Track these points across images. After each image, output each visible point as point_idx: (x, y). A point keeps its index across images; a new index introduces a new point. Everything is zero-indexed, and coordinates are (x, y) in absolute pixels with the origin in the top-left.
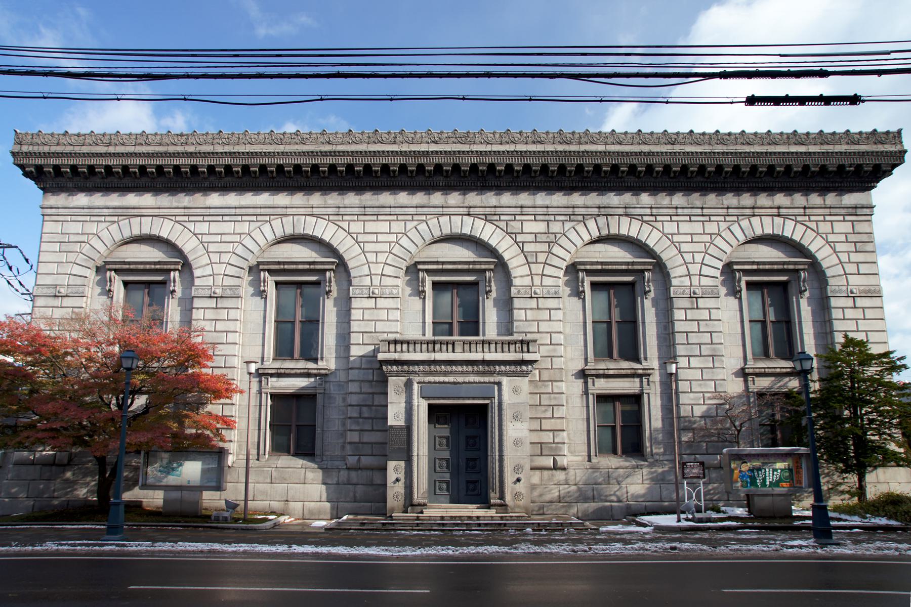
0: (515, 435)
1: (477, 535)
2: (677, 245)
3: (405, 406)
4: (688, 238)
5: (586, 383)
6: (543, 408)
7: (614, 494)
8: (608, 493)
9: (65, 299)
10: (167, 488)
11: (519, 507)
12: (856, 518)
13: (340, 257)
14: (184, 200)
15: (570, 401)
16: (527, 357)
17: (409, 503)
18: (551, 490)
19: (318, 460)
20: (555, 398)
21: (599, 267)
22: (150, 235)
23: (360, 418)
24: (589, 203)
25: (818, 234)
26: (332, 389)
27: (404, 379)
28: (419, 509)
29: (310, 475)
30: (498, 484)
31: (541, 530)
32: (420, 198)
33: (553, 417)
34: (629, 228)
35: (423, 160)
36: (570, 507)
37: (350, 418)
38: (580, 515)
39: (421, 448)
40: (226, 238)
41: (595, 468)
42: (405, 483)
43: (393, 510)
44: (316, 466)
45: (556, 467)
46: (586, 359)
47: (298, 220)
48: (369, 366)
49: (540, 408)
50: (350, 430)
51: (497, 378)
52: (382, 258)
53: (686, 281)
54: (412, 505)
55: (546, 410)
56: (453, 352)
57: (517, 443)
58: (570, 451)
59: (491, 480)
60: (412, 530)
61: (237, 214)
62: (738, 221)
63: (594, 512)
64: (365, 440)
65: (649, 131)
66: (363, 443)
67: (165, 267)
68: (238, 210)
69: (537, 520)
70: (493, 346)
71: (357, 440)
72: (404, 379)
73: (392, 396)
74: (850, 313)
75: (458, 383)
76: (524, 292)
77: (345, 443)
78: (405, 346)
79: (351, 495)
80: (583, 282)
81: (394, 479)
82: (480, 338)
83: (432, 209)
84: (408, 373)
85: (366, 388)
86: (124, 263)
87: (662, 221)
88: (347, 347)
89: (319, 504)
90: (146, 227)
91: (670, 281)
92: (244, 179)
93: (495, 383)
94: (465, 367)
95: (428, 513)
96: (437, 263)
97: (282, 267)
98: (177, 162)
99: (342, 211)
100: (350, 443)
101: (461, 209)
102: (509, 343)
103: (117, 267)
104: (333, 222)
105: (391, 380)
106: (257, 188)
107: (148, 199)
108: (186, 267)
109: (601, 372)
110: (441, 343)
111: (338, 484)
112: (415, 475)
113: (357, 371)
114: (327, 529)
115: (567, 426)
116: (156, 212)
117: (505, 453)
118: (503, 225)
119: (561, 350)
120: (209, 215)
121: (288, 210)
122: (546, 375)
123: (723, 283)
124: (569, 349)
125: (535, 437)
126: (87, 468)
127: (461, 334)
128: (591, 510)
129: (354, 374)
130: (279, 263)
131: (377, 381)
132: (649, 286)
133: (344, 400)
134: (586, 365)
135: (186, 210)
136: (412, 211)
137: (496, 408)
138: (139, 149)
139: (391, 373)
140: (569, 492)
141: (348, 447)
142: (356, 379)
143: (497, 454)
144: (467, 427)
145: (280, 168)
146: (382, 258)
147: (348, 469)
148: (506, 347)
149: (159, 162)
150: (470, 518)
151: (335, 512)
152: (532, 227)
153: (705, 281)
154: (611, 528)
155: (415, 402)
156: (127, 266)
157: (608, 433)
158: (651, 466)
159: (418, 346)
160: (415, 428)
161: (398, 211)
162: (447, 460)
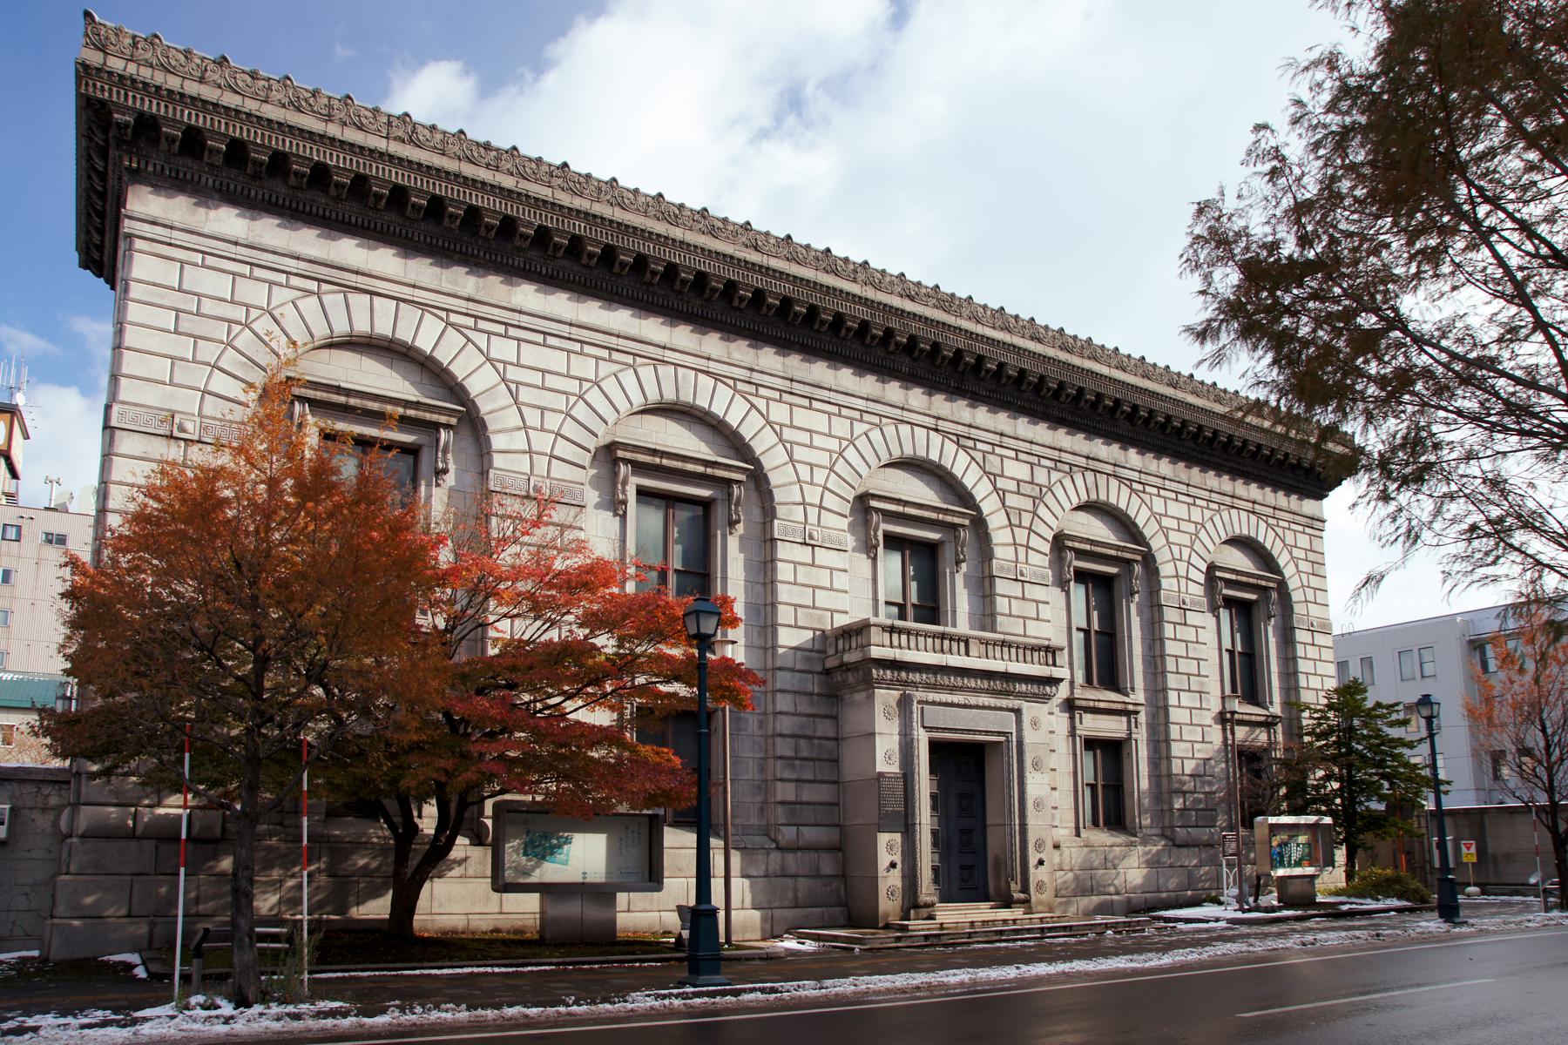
2: (789, 447)
4: (536, 378)
9: (195, 448)
10: (545, 889)
12: (1369, 901)
13: (756, 462)
14: (461, 280)
17: (911, 903)
21: (1088, 547)
22: (391, 341)
23: (796, 758)
24: (1077, 449)
25: (768, 422)
27: (896, 694)
32: (869, 384)
34: (1118, 497)
35: (894, 324)
36: (1068, 903)
40: (552, 381)
47: (684, 376)
48: (807, 668)
52: (553, 421)
53: (523, 464)
56: (967, 654)
61: (577, 338)
62: (633, 367)
64: (805, 797)
65: (804, 243)
66: (801, 803)
67: (428, 416)
68: (574, 330)
71: (792, 798)
72: (896, 694)
74: (1017, 608)
75: (971, 707)
76: (1008, 571)
79: (790, 894)
80: (625, 483)
81: (887, 864)
83: (888, 409)
84: (906, 683)
85: (804, 707)
86: (338, 390)
87: (489, 333)
90: (383, 320)
91: (1159, 583)
92: (595, 272)
96: (898, 501)
97: (657, 460)
98: (477, 200)
99: (757, 377)
101: (927, 419)
103: (319, 395)
104: (743, 395)
106: (612, 296)
107: (384, 260)
108: (473, 424)
109: (1091, 704)
113: (789, 675)
114: (814, 953)
116: (406, 292)
118: (978, 457)
120: (514, 325)
121: (667, 353)
123: (595, 483)
126: (270, 848)
127: (916, 620)
130: (654, 452)
131: (819, 695)
132: (445, 461)
135: (471, 305)
136: (861, 404)
138: (396, 148)
142: (788, 687)
145: (672, 269)
146: (553, 421)
149: (440, 189)
152: (1019, 470)
153: (559, 471)
156: (342, 399)
158: (1144, 843)
161: (841, 399)
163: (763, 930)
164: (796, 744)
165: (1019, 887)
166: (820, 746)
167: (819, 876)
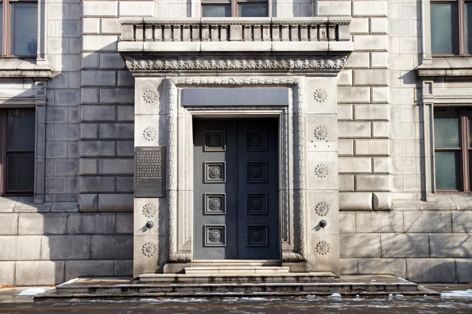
0: (317, 163)
1: (257, 303)
3: (159, 119)
5: (420, 89)
6: (358, 124)
7: (460, 246)
8: (450, 245)
11: (323, 263)
15: (396, 115)
16: (335, 46)
17: (165, 258)
18: (369, 240)
19: (38, 200)
20: (375, 110)
23: (98, 139)
26: (58, 99)
27: (158, 80)
28: (179, 267)
29: (25, 222)
30: (292, 230)
31: (354, 296)
33: (372, 137)
37: (83, 140)
38: (410, 275)
39: (182, 179)
41: (434, 210)
42: (160, 230)
43: (142, 269)
44: (35, 209)
45: (375, 208)
46: (420, 55)
49: (353, 124)
50: (84, 157)
51: (291, 79)
54: (170, 262)
55: (362, 127)
57: (320, 171)
58: (395, 186)
59: (282, 224)
60: (165, 296)
63: (430, 271)
64: (105, 170)
66: (102, 175)
69: (348, 280)
70: (285, 31)
72: (158, 80)
73: (140, 104)
75: (236, 85)
77: (76, 176)
78: (158, 32)
79: (85, 249)
81: (144, 224)
82: (268, 19)
84: (164, 71)
85: (106, 97)
88: (79, 40)
89: (37, 263)
93: (288, 85)
94: (245, 62)
95: (191, 272)
100: (83, 176)
102: (309, 27)
105: (141, 83)
109: (442, 73)
110: (210, 28)
111: (66, 234)
112: (177, 219)
113: (93, 73)
115: (392, 149)
117: (303, 186)
119: (383, 42)
122: (362, 77)
124: (395, 40)
125: (346, 166)
128: (426, 269)
129: (89, 78)
131: (121, 87)
133: (76, 114)
134: (420, 63)
137: (291, 121)
139: (139, 71)
140: (394, 243)
141: (81, 181)
143: (291, 187)
144: (249, 148)
147: (81, 212)
148: (304, 32)
150: (251, 278)
151: (61, 274)
154: (458, 294)
155: (173, 114)
157: (450, 160)
159: (177, 32)
160: (173, 151)
162: (221, 197)
163: (57, 277)
164: (98, 128)
165: (292, 246)
166: (121, 129)
167: (115, 234)
